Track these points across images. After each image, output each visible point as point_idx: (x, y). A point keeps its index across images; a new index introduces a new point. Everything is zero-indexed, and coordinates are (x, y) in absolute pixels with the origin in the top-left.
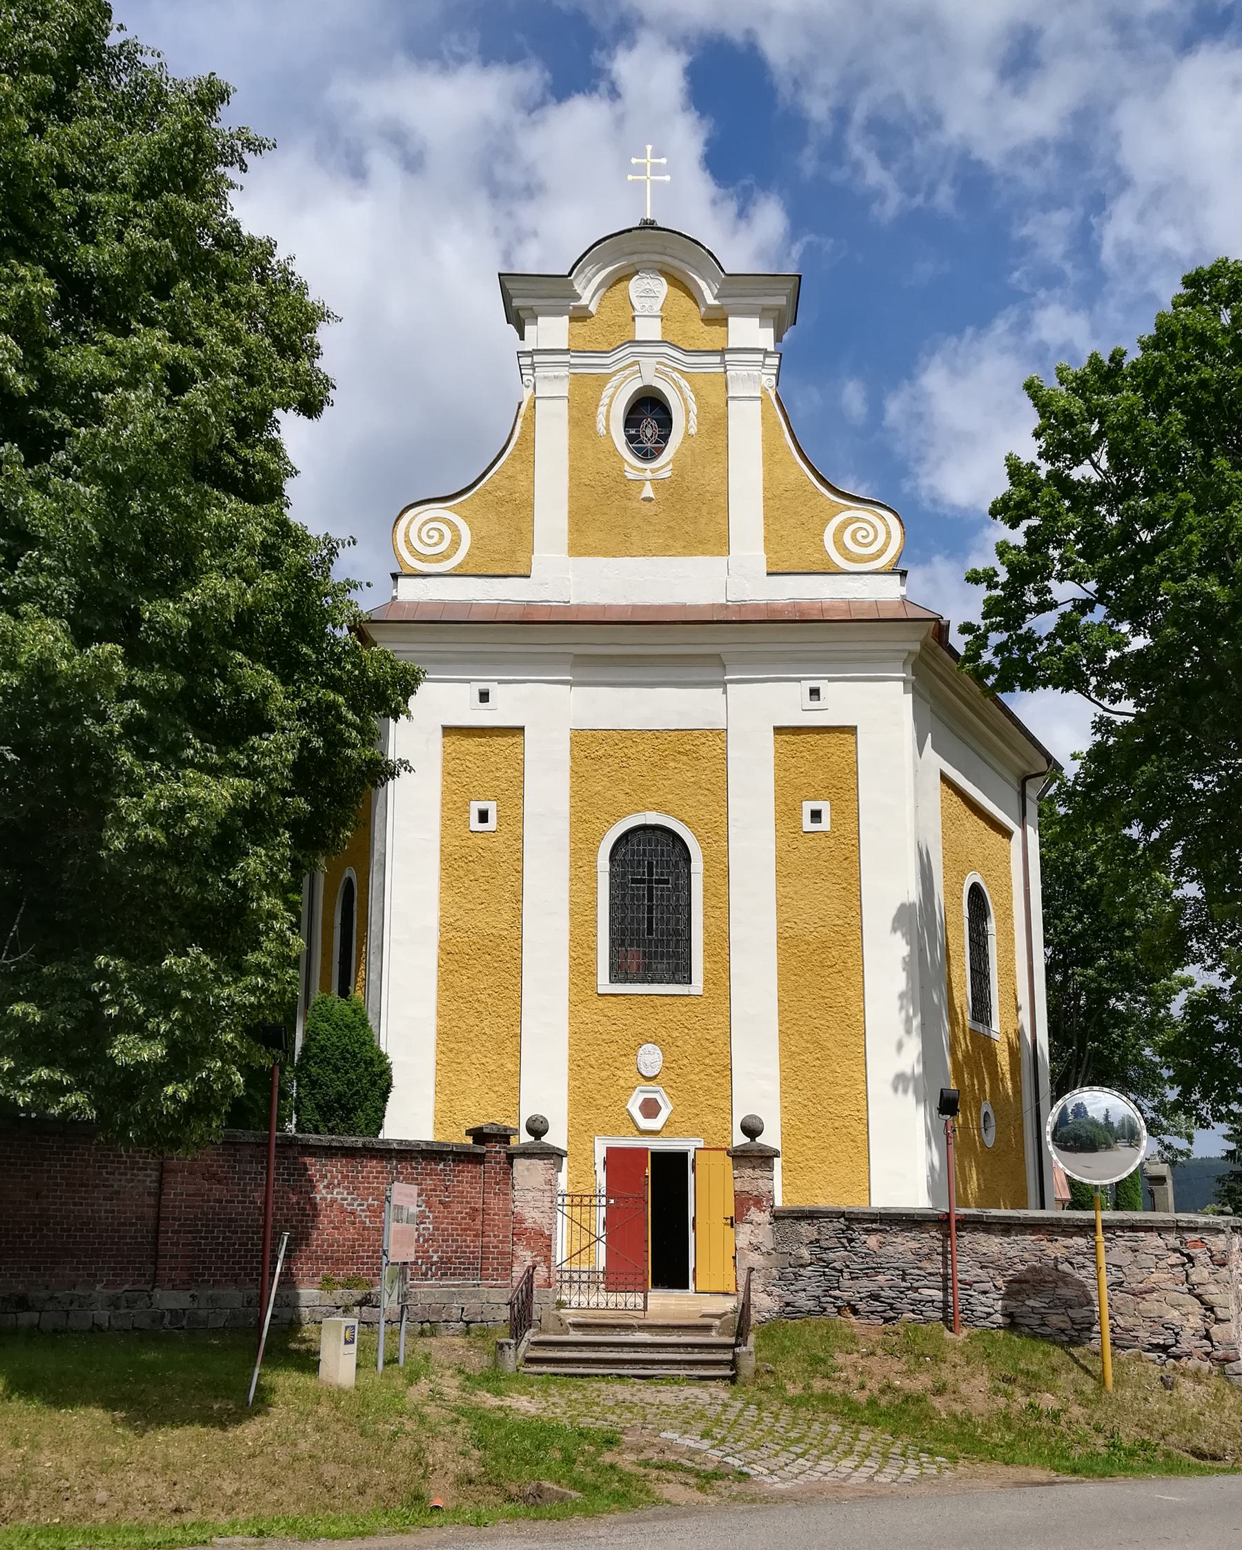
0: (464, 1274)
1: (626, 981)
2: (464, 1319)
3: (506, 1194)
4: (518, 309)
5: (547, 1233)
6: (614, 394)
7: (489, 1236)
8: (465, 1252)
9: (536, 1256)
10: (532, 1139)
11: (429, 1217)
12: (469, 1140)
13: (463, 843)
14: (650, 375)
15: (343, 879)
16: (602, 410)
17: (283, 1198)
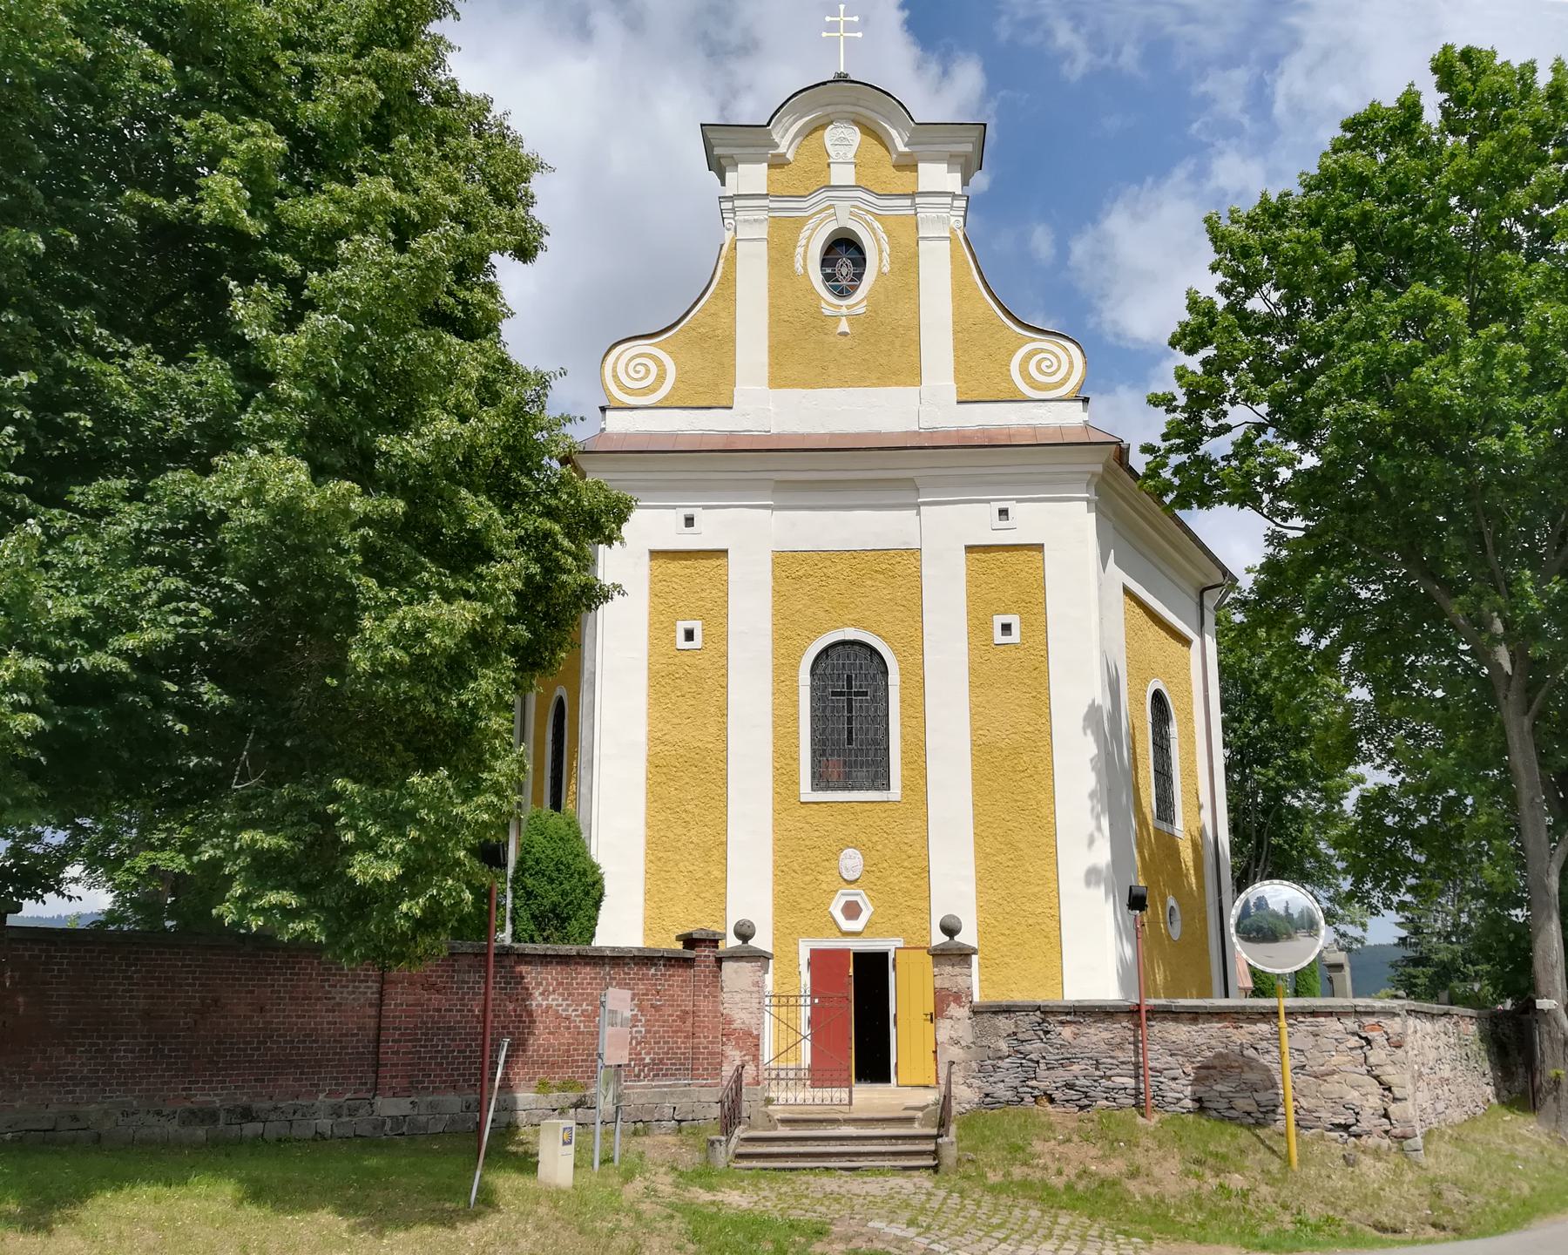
1: (827, 788)
4: (720, 157)
5: (755, 1033)
6: (811, 236)
10: (740, 942)
12: (679, 946)
13: (670, 661)
16: (800, 250)
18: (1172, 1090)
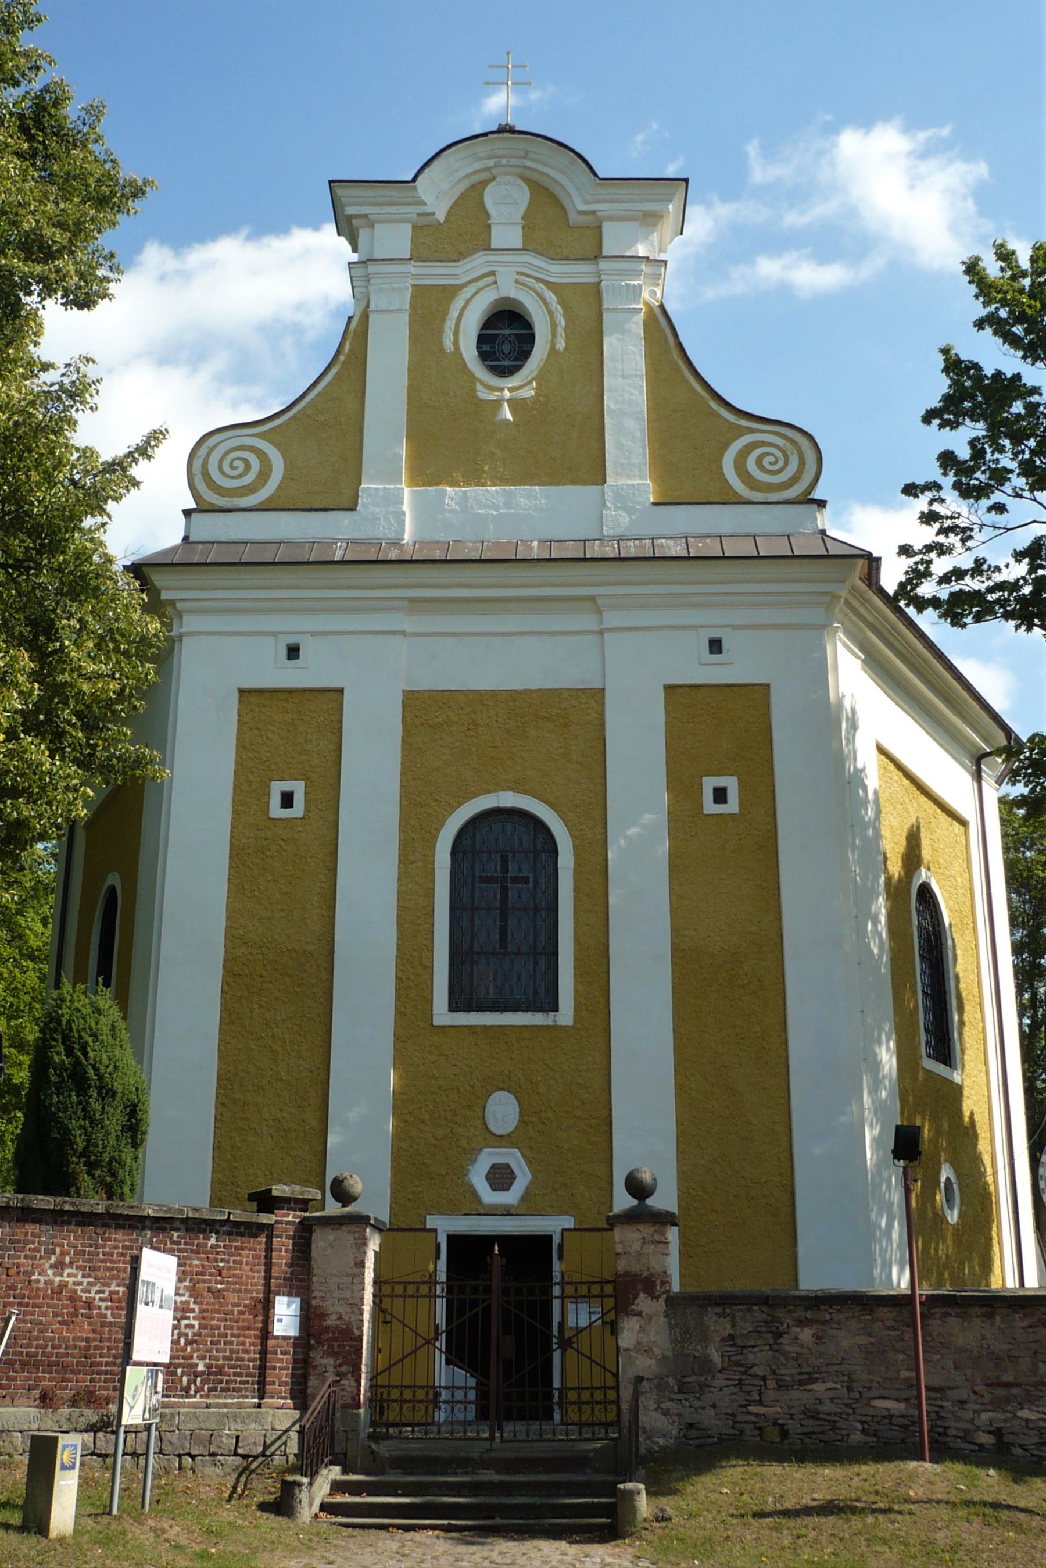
0: (239, 1390)
1: (468, 1009)
2: (240, 1451)
4: (350, 218)
8: (242, 1359)
9: (340, 1365)
11: (193, 1311)
14: (508, 288)
15: (105, 888)
16: (450, 324)
18: (958, 1419)
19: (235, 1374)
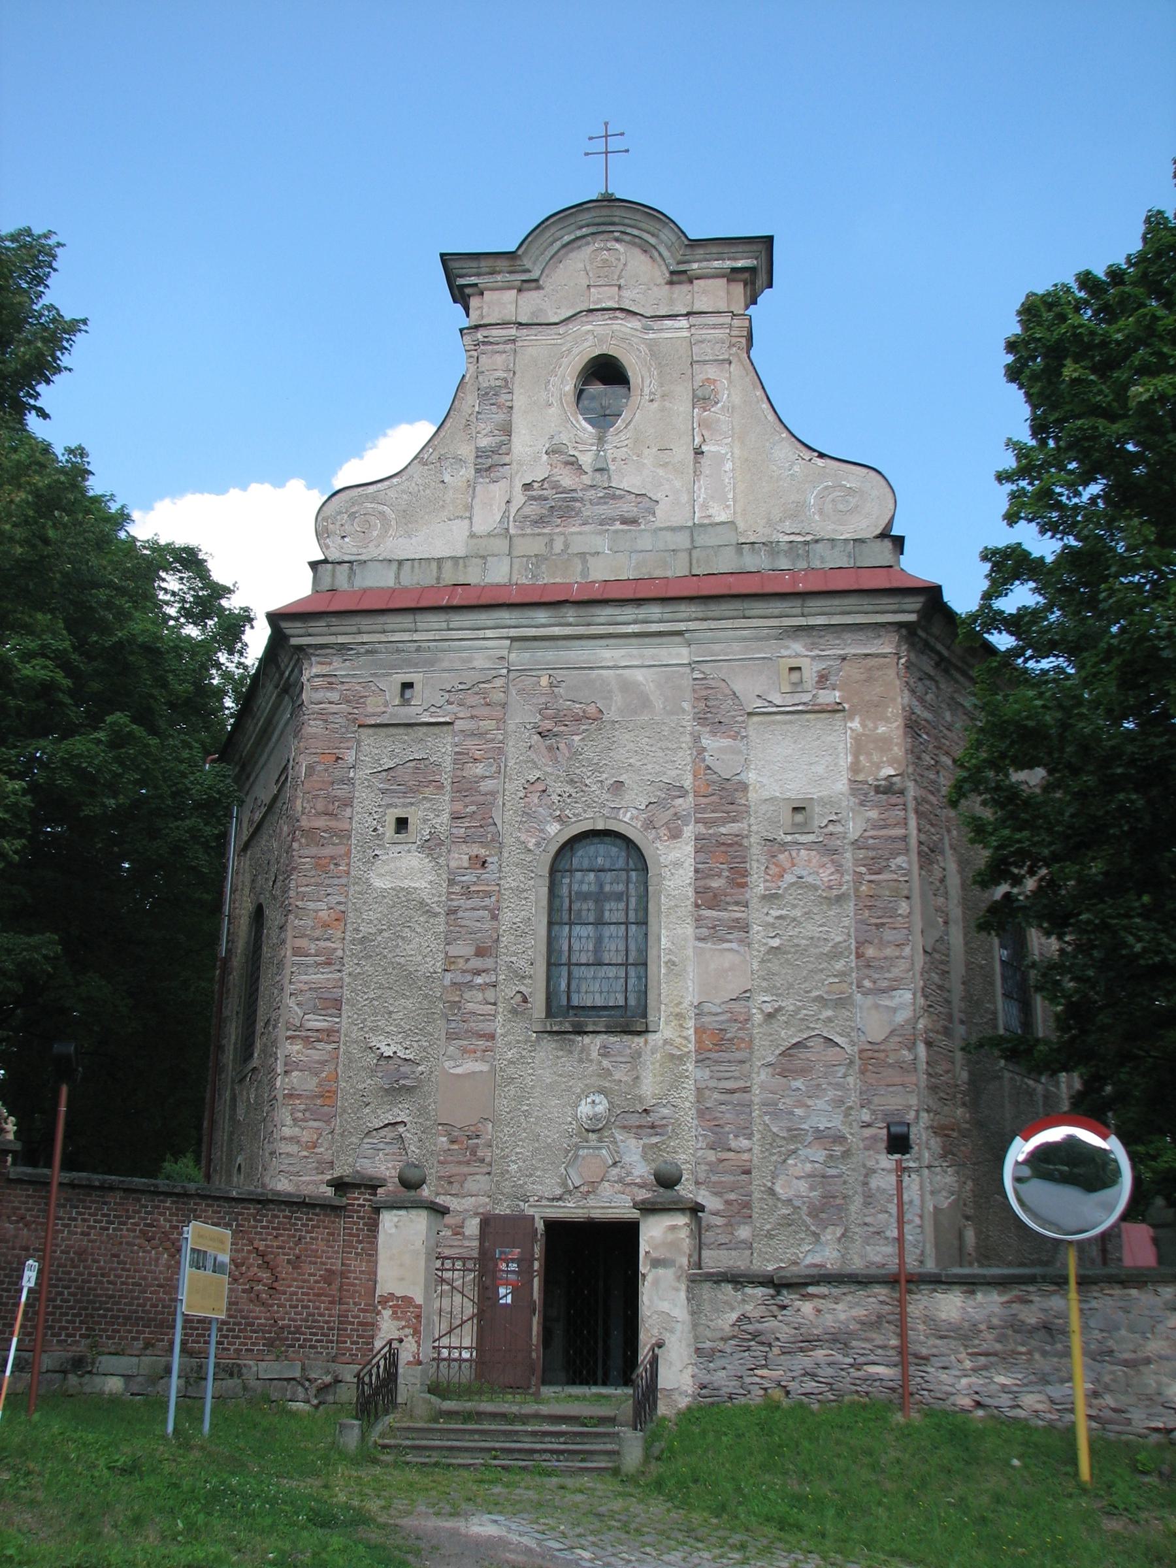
3: (370, 1255)
7: (348, 1304)
12: (329, 1192)
17: (100, 1249)
19: (311, 1334)
